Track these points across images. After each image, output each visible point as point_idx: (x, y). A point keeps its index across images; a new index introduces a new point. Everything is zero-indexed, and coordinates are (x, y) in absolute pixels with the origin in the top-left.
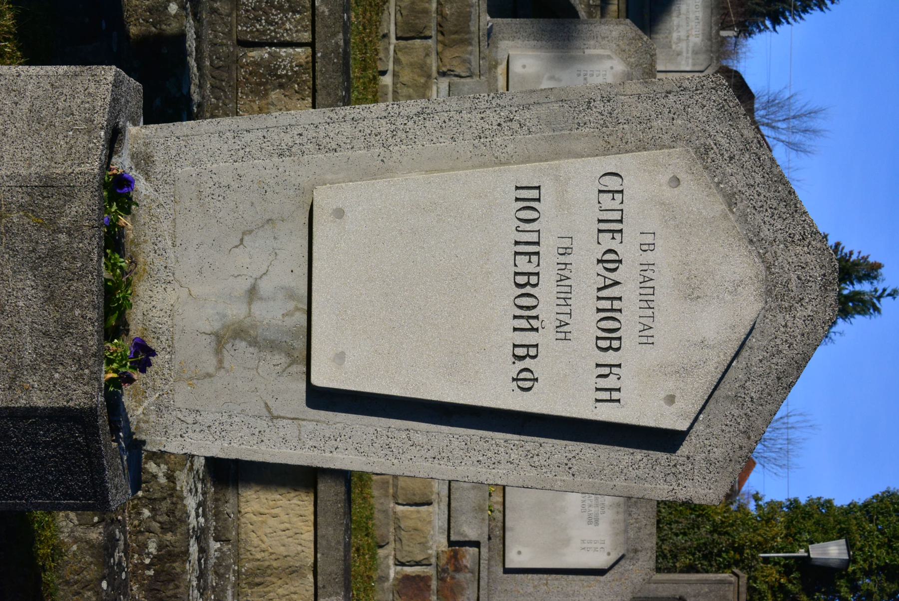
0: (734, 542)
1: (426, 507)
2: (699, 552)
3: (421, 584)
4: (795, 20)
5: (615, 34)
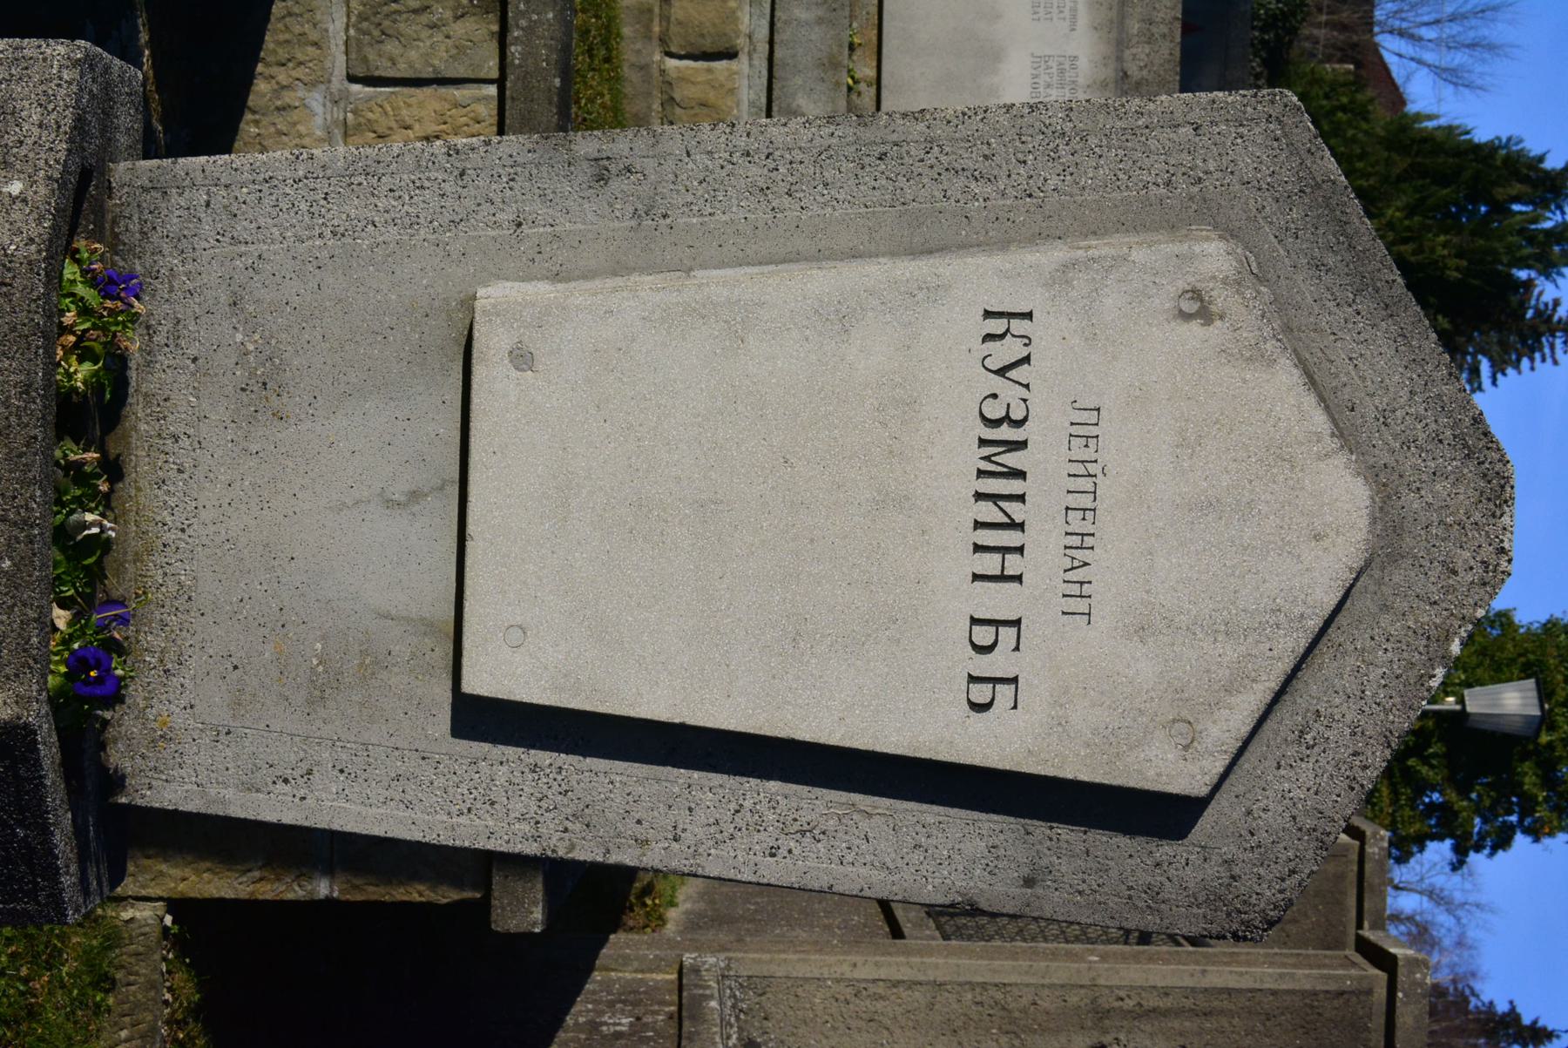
1: (724, 63)
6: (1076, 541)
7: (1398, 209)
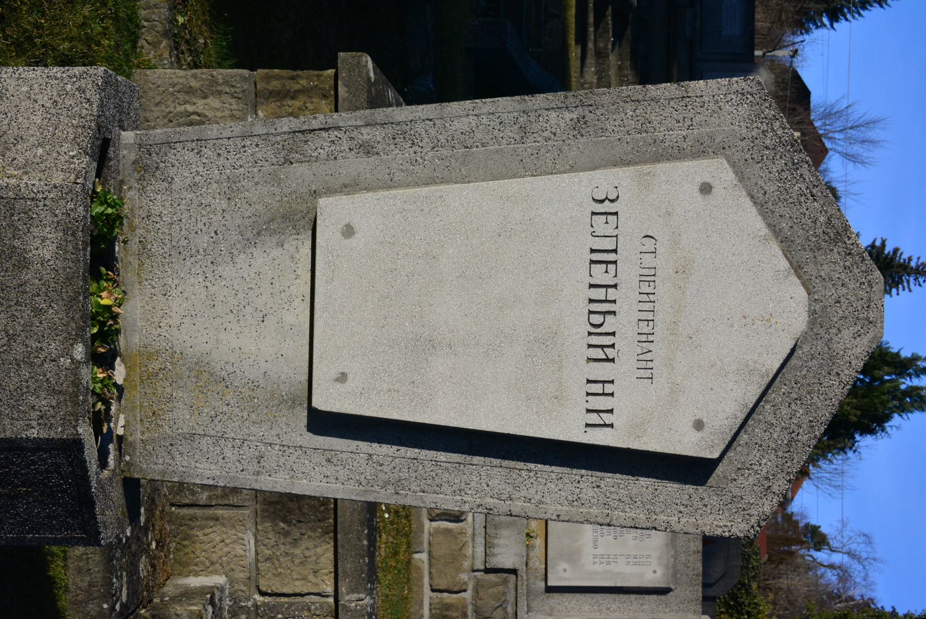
4: (854, 17)
6: (644, 338)
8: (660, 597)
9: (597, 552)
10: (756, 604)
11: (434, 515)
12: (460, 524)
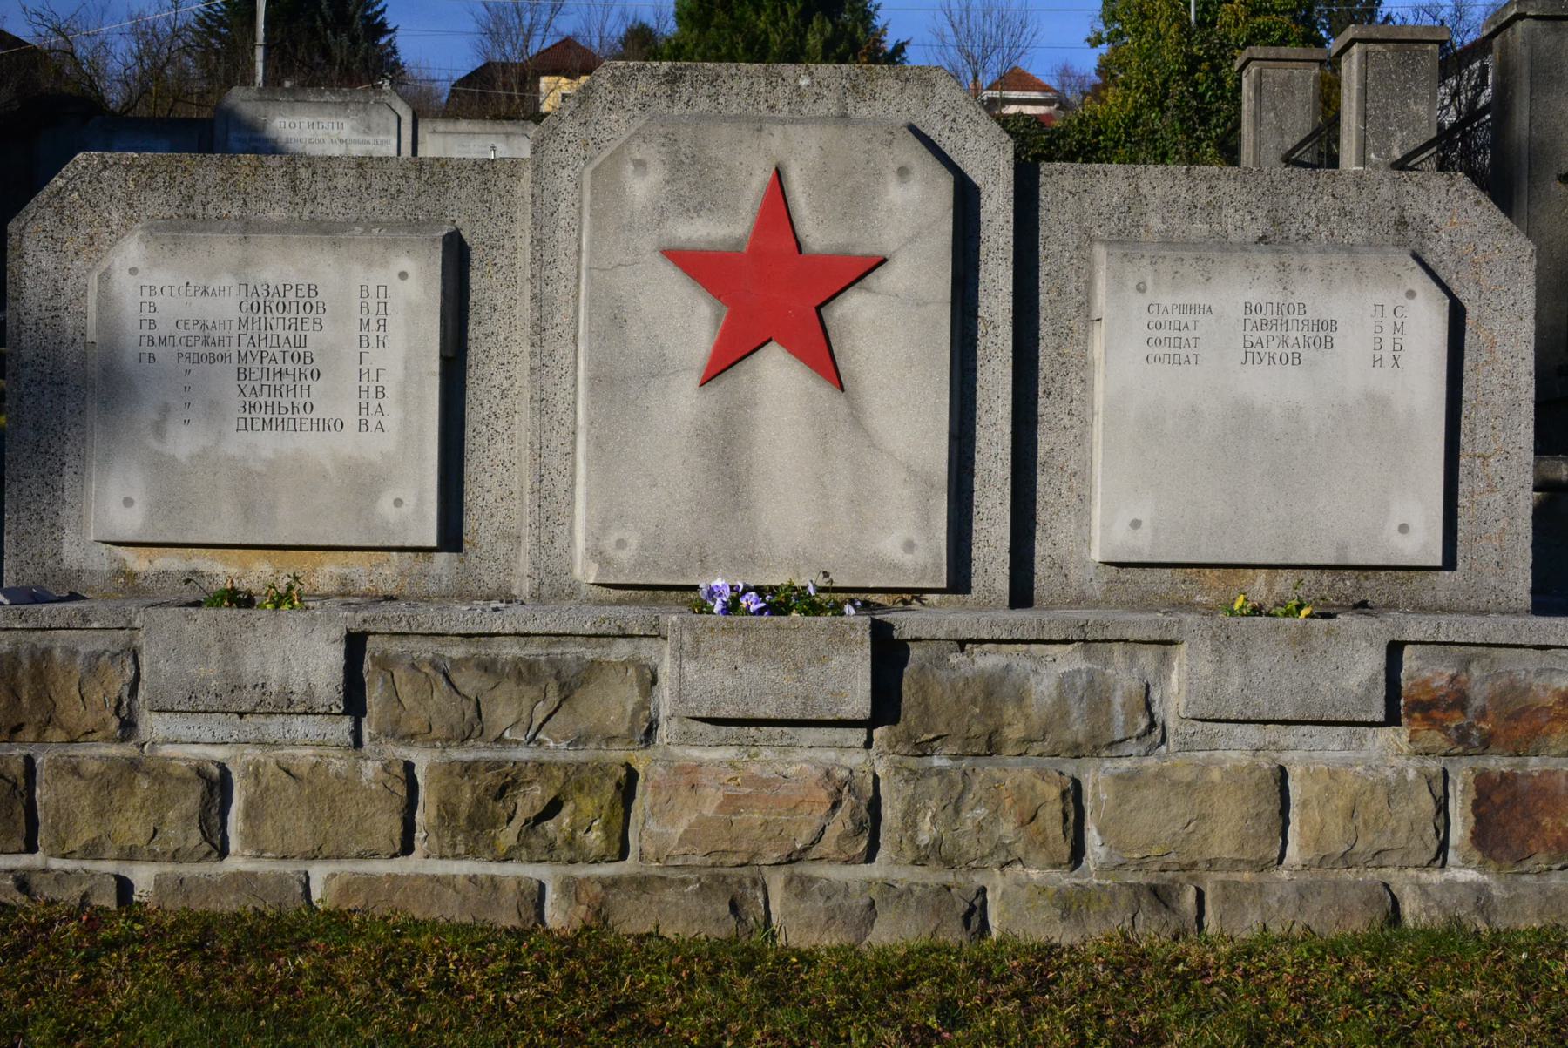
0: (1180, 72)
1: (1290, 783)
2: (1195, 130)
3: (1497, 798)
5: (47, 261)
7: (759, 17)
8: (475, 263)
9: (351, 420)
10: (1081, 122)
11: (206, 847)
12: (235, 777)
